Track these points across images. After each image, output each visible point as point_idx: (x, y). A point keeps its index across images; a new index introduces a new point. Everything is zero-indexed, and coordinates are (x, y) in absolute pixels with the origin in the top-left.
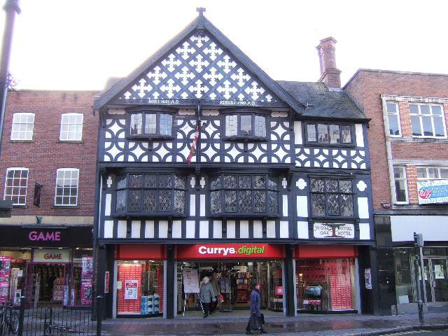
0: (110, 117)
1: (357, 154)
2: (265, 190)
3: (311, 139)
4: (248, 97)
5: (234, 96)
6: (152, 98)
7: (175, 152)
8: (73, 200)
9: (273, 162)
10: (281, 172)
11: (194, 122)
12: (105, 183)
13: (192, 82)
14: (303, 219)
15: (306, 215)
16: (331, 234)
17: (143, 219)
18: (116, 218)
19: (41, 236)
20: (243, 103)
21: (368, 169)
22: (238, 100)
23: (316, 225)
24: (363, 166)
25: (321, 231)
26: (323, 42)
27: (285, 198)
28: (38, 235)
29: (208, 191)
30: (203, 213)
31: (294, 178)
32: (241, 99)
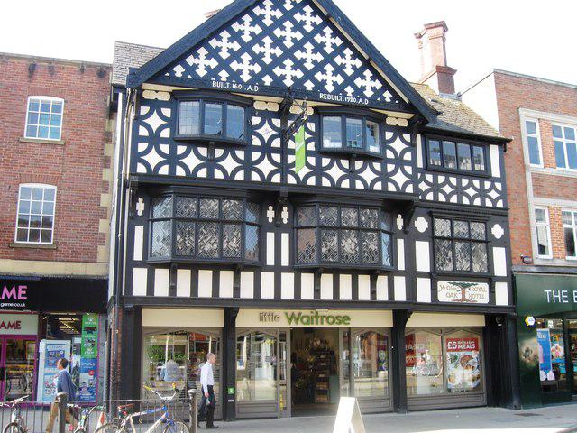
4: (359, 91)
5: (339, 89)
6: (218, 79)
8: (46, 237)
9: (324, 184)
10: (401, 206)
14: (423, 275)
15: (427, 269)
16: (459, 297)
18: (152, 265)
20: (353, 100)
21: (506, 209)
23: (441, 283)
24: (500, 204)
29: (293, 228)
30: (285, 262)
31: (414, 216)
32: (349, 94)
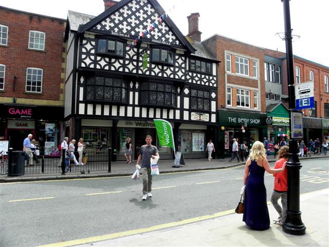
2: (157, 91)
5: (160, 38)
6: (114, 31)
7: (124, 66)
9: (97, 68)
11: (136, 50)
12: (79, 80)
13: (137, 26)
14: (186, 110)
17: (103, 105)
18: (86, 102)
19: (18, 111)
20: (165, 43)
22: (162, 40)
24: (215, 85)
25: (195, 117)
26: (193, 14)
28: (15, 110)
30: (136, 103)
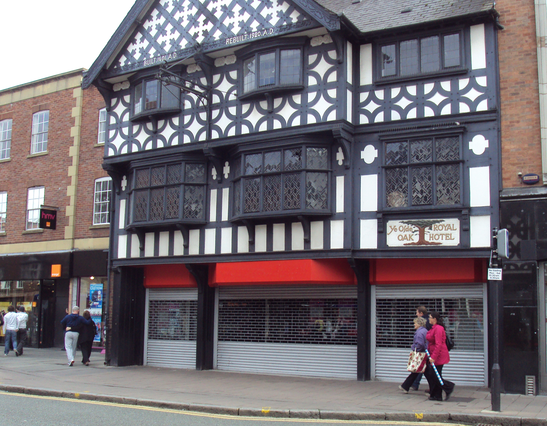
0: (216, 70)
1: (473, 85)
3: (388, 71)
9: (426, 115)
14: (369, 215)
16: (416, 239)
23: (391, 224)
27: (340, 181)
29: (234, 183)
30: (225, 217)
